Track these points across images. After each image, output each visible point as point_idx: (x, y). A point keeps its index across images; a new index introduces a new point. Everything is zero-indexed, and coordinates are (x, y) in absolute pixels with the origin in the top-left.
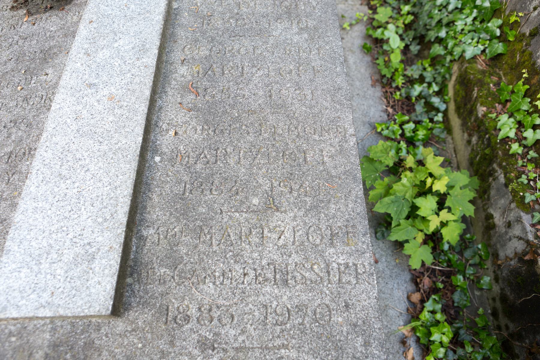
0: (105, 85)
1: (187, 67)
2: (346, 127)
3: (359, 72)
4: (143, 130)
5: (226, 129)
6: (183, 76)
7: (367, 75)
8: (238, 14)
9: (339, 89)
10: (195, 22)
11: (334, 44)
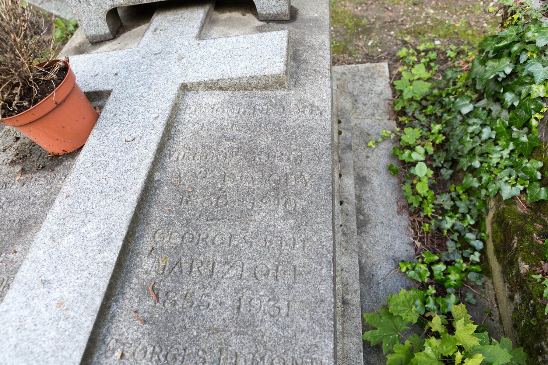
0: (59, 283)
1: (153, 260)
2: (324, 361)
3: (384, 195)
4: (81, 357)
5: (179, 355)
6: (147, 272)
7: (393, 200)
8: (221, 189)
9: (322, 301)
10: (173, 199)
11: (323, 235)
